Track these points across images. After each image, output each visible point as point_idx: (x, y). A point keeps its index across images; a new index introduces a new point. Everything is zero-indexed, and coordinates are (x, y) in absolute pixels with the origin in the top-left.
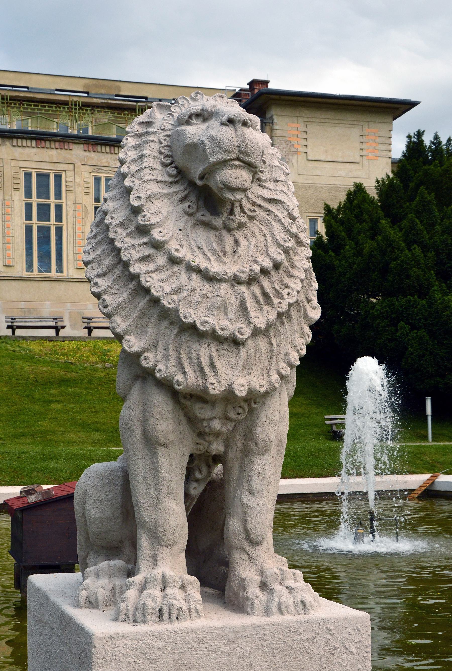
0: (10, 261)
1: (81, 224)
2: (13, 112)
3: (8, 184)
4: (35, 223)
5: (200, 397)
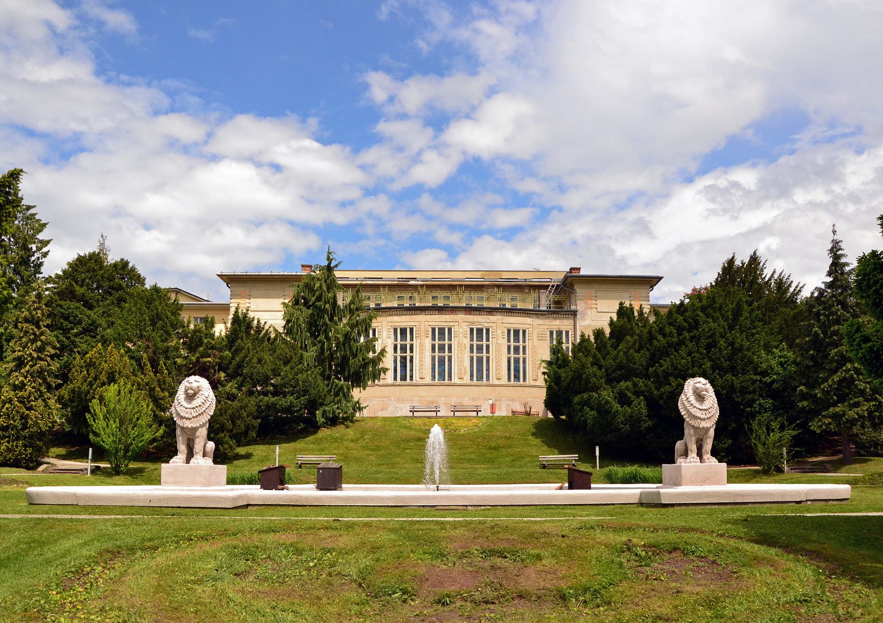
3: (423, 334)
4: (512, 355)
5: (698, 428)
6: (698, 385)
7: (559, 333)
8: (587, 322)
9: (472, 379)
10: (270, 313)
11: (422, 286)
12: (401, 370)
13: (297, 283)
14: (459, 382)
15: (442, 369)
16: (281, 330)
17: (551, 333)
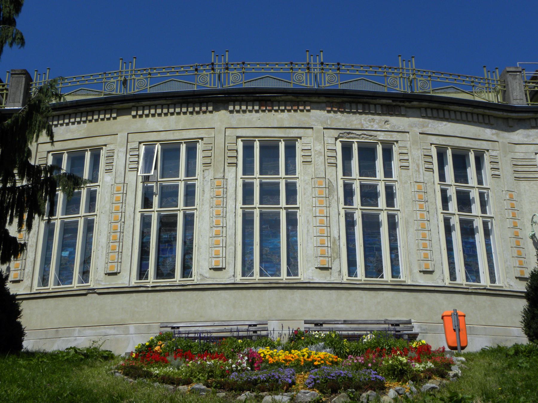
0: (219, 261)
1: (325, 205)
2: (232, 74)
12: (148, 243)
14: (319, 278)
15: (269, 239)
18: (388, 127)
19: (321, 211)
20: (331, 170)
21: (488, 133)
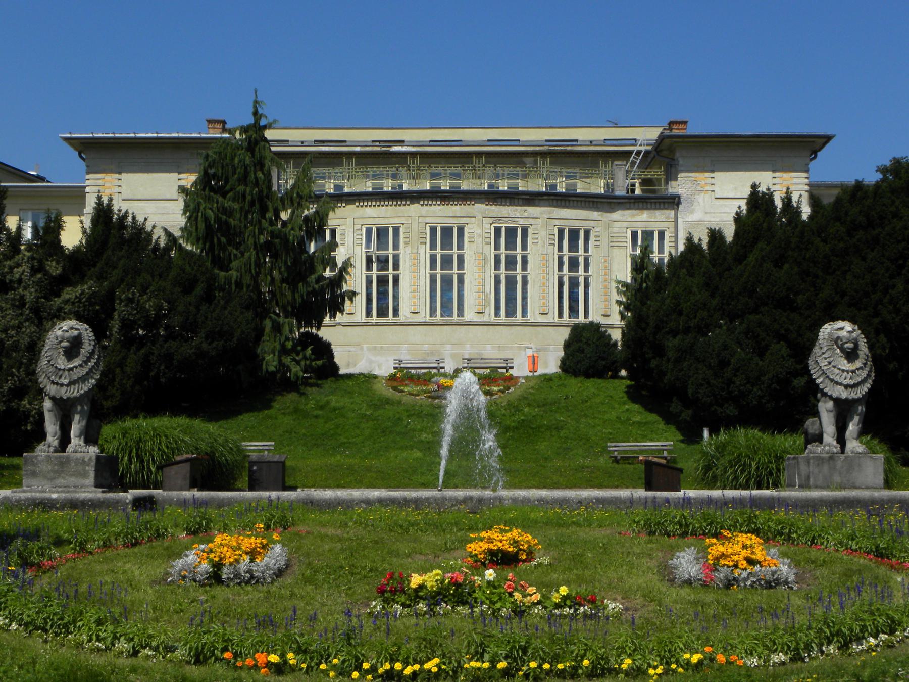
6: (843, 334)
7: (648, 235)
8: (697, 216)
9: (497, 314)
10: (157, 202)
11: (413, 154)
13: (204, 152)
15: (446, 294)
16: (177, 234)
17: (634, 235)
18: (526, 215)
19: (479, 276)
20: (487, 247)
21: (595, 215)
